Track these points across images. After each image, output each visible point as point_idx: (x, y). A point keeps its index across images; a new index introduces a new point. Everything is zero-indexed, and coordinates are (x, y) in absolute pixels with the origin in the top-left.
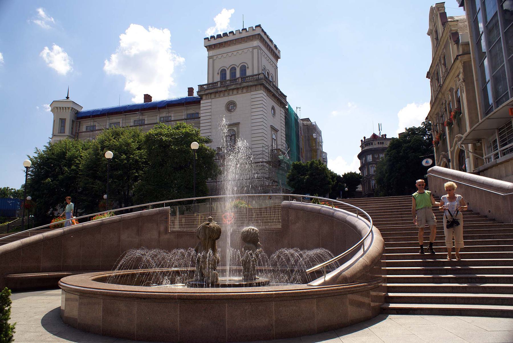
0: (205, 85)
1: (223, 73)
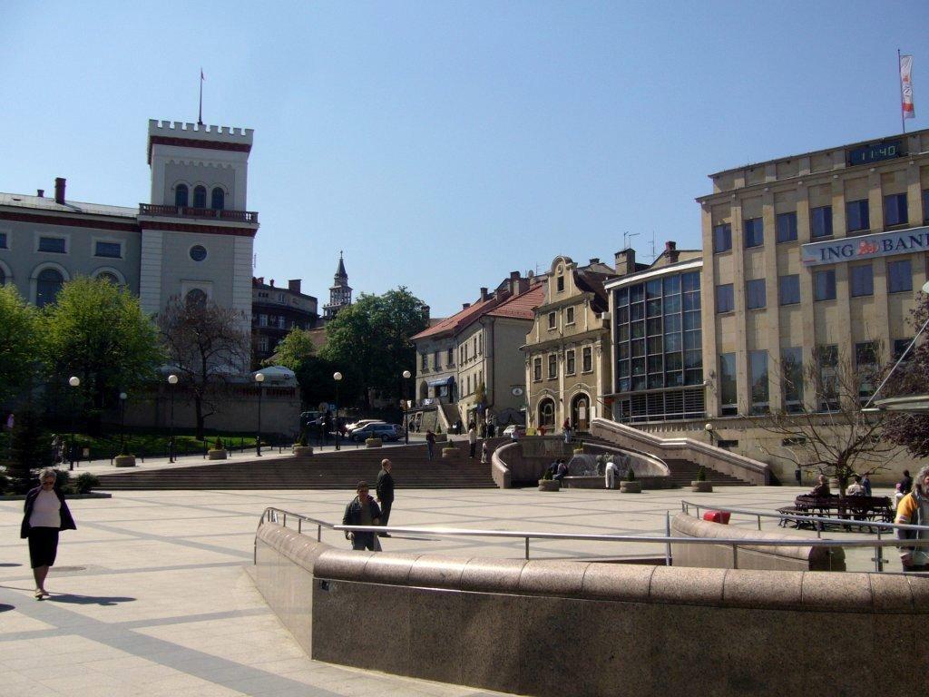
0: (146, 205)
1: (181, 191)
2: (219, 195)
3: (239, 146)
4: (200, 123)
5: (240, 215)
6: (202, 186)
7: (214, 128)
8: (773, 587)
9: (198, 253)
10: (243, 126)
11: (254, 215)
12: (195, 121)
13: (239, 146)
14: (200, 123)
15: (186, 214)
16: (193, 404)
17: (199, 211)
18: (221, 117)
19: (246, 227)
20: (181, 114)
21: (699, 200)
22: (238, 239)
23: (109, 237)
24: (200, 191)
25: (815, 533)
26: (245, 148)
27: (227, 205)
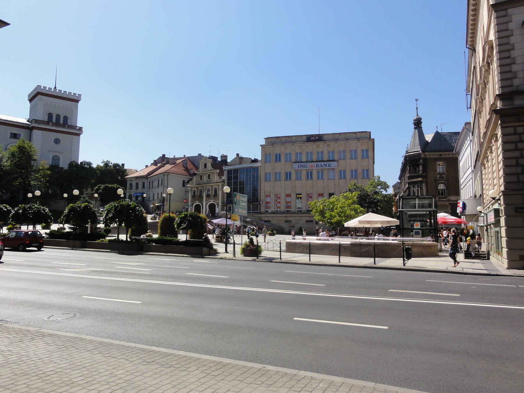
1: (50, 115)
2: (66, 118)
3: (75, 100)
4: (55, 88)
5: (74, 127)
6: (56, 113)
7: (60, 91)
8: (106, 164)
9: (57, 141)
10: (77, 93)
11: (80, 129)
12: (53, 88)
13: (75, 100)
14: (55, 88)
15: (54, 124)
16: (224, 245)
17: (57, 124)
18: (65, 87)
19: (77, 132)
20: (48, 84)
21: (238, 155)
22: (74, 137)
23: (16, 131)
24: (58, 116)
25: (291, 237)
26: (77, 101)
27: (69, 123)
